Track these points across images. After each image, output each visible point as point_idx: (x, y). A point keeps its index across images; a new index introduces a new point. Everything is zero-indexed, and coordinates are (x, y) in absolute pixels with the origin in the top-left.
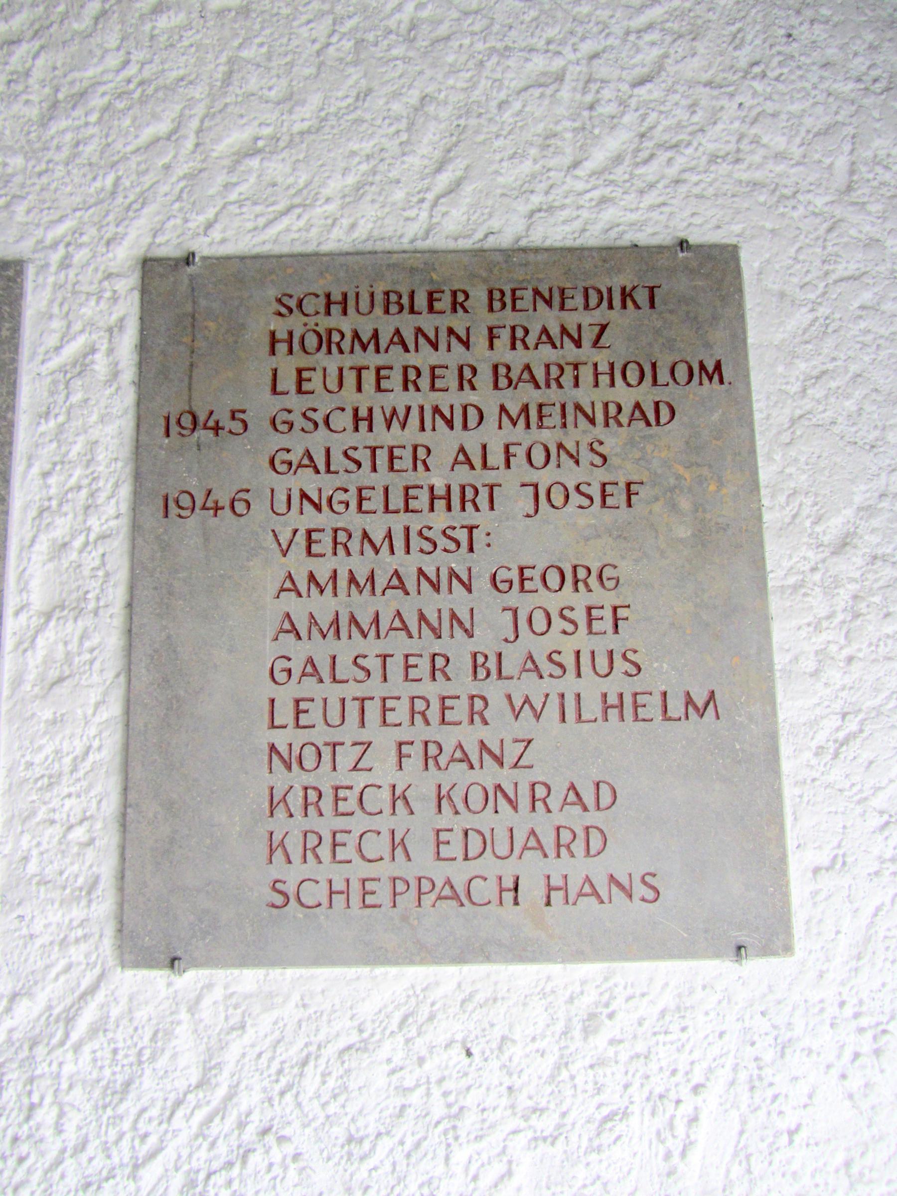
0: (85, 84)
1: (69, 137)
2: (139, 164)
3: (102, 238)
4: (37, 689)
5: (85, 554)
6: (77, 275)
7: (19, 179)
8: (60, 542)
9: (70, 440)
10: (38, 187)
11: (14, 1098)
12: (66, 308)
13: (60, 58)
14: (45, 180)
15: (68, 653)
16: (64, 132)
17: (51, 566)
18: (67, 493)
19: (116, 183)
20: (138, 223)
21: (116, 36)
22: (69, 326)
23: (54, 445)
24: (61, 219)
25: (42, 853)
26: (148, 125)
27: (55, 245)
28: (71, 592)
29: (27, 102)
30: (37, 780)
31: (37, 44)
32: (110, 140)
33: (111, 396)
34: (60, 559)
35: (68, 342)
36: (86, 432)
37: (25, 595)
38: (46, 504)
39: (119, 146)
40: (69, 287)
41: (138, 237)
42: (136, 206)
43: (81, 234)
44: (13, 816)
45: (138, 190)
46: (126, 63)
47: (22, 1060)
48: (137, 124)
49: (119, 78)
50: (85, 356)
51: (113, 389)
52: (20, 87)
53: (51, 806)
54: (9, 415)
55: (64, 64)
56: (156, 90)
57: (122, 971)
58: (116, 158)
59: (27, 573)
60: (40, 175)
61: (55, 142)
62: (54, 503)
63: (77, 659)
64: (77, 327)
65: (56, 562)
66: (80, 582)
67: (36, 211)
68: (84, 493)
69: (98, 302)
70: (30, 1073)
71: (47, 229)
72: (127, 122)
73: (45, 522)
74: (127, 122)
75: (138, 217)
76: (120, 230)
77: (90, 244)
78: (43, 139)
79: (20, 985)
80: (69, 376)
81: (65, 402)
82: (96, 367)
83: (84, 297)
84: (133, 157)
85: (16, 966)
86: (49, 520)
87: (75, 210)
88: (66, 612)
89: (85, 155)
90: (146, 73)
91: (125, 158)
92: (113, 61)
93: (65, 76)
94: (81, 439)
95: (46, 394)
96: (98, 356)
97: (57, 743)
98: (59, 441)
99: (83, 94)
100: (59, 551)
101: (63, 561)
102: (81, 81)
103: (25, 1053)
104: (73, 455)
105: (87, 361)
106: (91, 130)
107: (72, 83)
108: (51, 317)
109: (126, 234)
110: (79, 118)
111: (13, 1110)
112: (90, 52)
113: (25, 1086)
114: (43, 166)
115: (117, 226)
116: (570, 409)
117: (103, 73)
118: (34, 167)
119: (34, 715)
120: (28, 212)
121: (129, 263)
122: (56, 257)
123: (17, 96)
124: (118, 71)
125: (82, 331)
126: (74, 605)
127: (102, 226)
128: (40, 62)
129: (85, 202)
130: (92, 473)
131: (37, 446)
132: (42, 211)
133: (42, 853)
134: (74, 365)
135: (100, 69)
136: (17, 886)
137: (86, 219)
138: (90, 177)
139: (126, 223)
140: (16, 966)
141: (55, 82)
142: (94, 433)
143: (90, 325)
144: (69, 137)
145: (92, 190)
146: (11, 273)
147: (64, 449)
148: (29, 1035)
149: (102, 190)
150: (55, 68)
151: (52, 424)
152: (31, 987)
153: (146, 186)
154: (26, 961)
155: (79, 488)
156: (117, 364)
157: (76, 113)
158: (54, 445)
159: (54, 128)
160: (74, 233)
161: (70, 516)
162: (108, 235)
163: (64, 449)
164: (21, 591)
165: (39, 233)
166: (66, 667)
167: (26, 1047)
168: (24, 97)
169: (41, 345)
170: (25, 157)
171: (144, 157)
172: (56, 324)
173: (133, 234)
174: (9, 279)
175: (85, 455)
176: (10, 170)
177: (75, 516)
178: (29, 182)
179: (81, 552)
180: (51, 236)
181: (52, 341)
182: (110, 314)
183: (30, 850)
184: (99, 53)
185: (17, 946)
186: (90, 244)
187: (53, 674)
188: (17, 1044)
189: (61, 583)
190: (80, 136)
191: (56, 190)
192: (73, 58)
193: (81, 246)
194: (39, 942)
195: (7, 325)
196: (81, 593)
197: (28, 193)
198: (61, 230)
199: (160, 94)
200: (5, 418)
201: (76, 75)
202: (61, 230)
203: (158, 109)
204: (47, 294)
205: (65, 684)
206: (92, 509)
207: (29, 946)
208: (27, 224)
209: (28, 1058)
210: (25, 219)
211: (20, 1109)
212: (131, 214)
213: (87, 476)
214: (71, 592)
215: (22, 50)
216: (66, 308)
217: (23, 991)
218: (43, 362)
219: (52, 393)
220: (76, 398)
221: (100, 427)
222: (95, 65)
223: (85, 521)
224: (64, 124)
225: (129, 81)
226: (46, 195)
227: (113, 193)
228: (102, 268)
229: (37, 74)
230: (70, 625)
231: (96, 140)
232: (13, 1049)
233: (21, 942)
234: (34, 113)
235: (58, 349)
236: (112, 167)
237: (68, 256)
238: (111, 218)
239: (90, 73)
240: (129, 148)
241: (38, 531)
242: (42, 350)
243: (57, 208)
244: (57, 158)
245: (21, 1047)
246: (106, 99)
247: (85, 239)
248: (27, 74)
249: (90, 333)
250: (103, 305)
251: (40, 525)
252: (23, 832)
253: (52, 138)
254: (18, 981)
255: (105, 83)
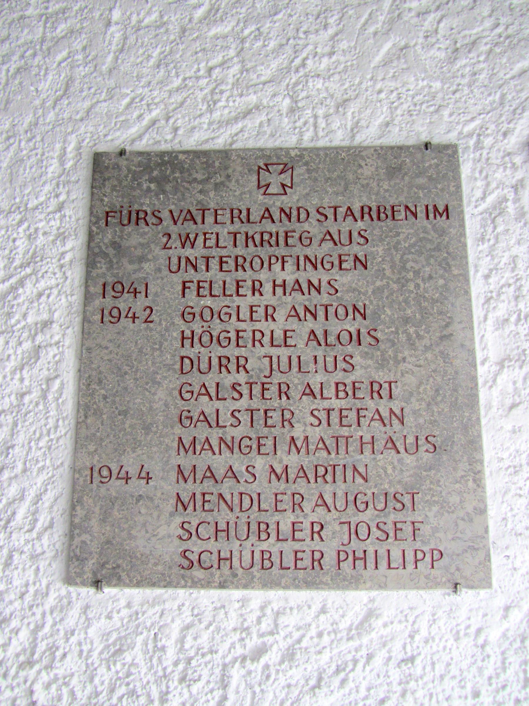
0: (473, 38)
1: (468, 69)
2: (515, 86)
3: (500, 131)
4: (500, 411)
5: (519, 326)
6: (488, 153)
7: (440, 95)
8: (502, 318)
9: (500, 255)
10: (453, 100)
11: (513, 674)
12: (484, 174)
13: (455, 22)
14: (457, 95)
15: (516, 389)
16: (465, 66)
17: (497, 333)
18: (501, 288)
19: (503, 97)
20: (521, 122)
21: (488, 9)
22: (488, 185)
23: (489, 258)
24: (473, 119)
25: (514, 516)
26: (518, 62)
27: (470, 135)
28: (512, 350)
29: (439, 49)
30: (507, 469)
31: (439, 14)
32: (495, 71)
33: (521, 228)
34: (503, 329)
35: (489, 194)
36: (509, 250)
37: (485, 351)
38: (489, 295)
39: (501, 75)
40: (483, 160)
41: (522, 130)
42: (519, 111)
43: (487, 129)
44: (495, 492)
45: (518, 101)
46: (497, 25)
47: (516, 649)
48: (511, 61)
49: (492, 35)
50: (500, 203)
51: (522, 224)
52: (434, 40)
53: (518, 485)
54: (462, 239)
55: (457, 26)
56: (519, 41)
57: (95, 594)
58: (501, 82)
59: (485, 338)
60: (454, 93)
61: (460, 73)
62: (494, 294)
63: (523, 392)
64: (494, 185)
65: (500, 331)
66: (519, 344)
67: (456, 114)
68: (512, 288)
69: (504, 170)
70: (523, 658)
71: (464, 125)
72: (504, 60)
73: (492, 306)
74: (504, 60)
75: (522, 118)
76: (511, 126)
77: (492, 134)
78: (452, 71)
79: (510, 601)
80: (493, 215)
81: (493, 232)
82: (509, 210)
83: (495, 167)
84: (511, 82)
85: (507, 588)
86: (495, 305)
87: (480, 114)
88: (513, 363)
89: (480, 81)
90: (510, 31)
91: (505, 83)
92: (488, 24)
93: (459, 33)
94: (507, 254)
95: (479, 227)
96: (509, 204)
97: (518, 445)
98: (492, 256)
99: (474, 43)
100: (503, 325)
101: (506, 330)
102: (470, 36)
103: (517, 644)
104: (501, 265)
105: (503, 206)
106: (482, 66)
107: (465, 36)
108: (476, 179)
109: (515, 128)
110: (473, 58)
111: (513, 681)
112: (475, 18)
113: (520, 666)
114: (455, 87)
115: (509, 123)
116: (302, 259)
117: (483, 31)
118: (449, 88)
119: (502, 427)
120: (451, 115)
121: (517, 147)
122: (472, 142)
123: (433, 45)
124: (492, 30)
125: (497, 188)
126: (516, 358)
127: (499, 124)
128: (442, 25)
129: (484, 109)
130: (517, 275)
131: (479, 259)
132: (459, 114)
133: (514, 516)
134: (494, 208)
135: (481, 29)
136: (504, 536)
137: (487, 119)
138: (486, 93)
139: (515, 121)
140: (507, 588)
141: (453, 36)
142: (515, 251)
143: (501, 185)
144: (468, 69)
145: (487, 102)
146: (450, 152)
147: (496, 261)
148: (517, 633)
149: (494, 102)
150: (452, 29)
151: (486, 245)
152: (518, 602)
153: (523, 99)
154: (513, 585)
155: (509, 285)
156: (523, 208)
157: (471, 56)
158: (489, 258)
159: (459, 63)
160: (481, 128)
161: (506, 302)
162: (503, 130)
163: (496, 261)
164: (483, 349)
165: (459, 127)
166: (516, 397)
167: (518, 640)
168: (437, 46)
169: (473, 196)
170: (442, 82)
171: (519, 82)
172: (479, 183)
173: (519, 128)
174: (450, 156)
175: (510, 264)
176: (433, 90)
177: (509, 302)
178: (446, 97)
179: (516, 325)
180: (467, 129)
181: (478, 194)
182: (513, 177)
183: (506, 513)
184: (479, 19)
185: (507, 575)
186: (492, 134)
187: (508, 402)
188: (512, 639)
189: (504, 344)
190: (475, 69)
191: (465, 102)
192: (464, 22)
193: (488, 135)
194: (520, 572)
195: (453, 184)
196: (520, 350)
197: (448, 104)
198: (472, 126)
199: (522, 43)
200: (460, 241)
201: (467, 32)
202: (472, 126)
203: (523, 52)
204: (470, 164)
205: (519, 407)
206: (520, 299)
207: (515, 575)
208: (451, 122)
209: (520, 648)
210: (448, 120)
211: (518, 681)
212: (517, 116)
213: (513, 277)
214: (512, 350)
215: (431, 18)
216: (484, 174)
217: (513, 605)
218: (476, 207)
219: (484, 226)
220: (500, 229)
221: (517, 246)
222: (479, 26)
223: (517, 306)
224: (464, 62)
225: (500, 36)
226: (459, 105)
227: (502, 104)
228: (502, 149)
229: (441, 32)
230: (517, 370)
231: (485, 71)
232: (508, 642)
233: (509, 573)
234: (442, 55)
235: (483, 198)
236: (500, 88)
237: (478, 142)
238: (503, 119)
239: (475, 31)
240: (508, 76)
241: (488, 311)
242: (474, 199)
243: (469, 113)
244: (462, 83)
245: (515, 640)
246: (488, 46)
247: (489, 131)
248: (436, 31)
249: (503, 189)
250: (508, 172)
251: (488, 307)
252: (503, 502)
253: (458, 71)
254: (509, 598)
255: (484, 37)
